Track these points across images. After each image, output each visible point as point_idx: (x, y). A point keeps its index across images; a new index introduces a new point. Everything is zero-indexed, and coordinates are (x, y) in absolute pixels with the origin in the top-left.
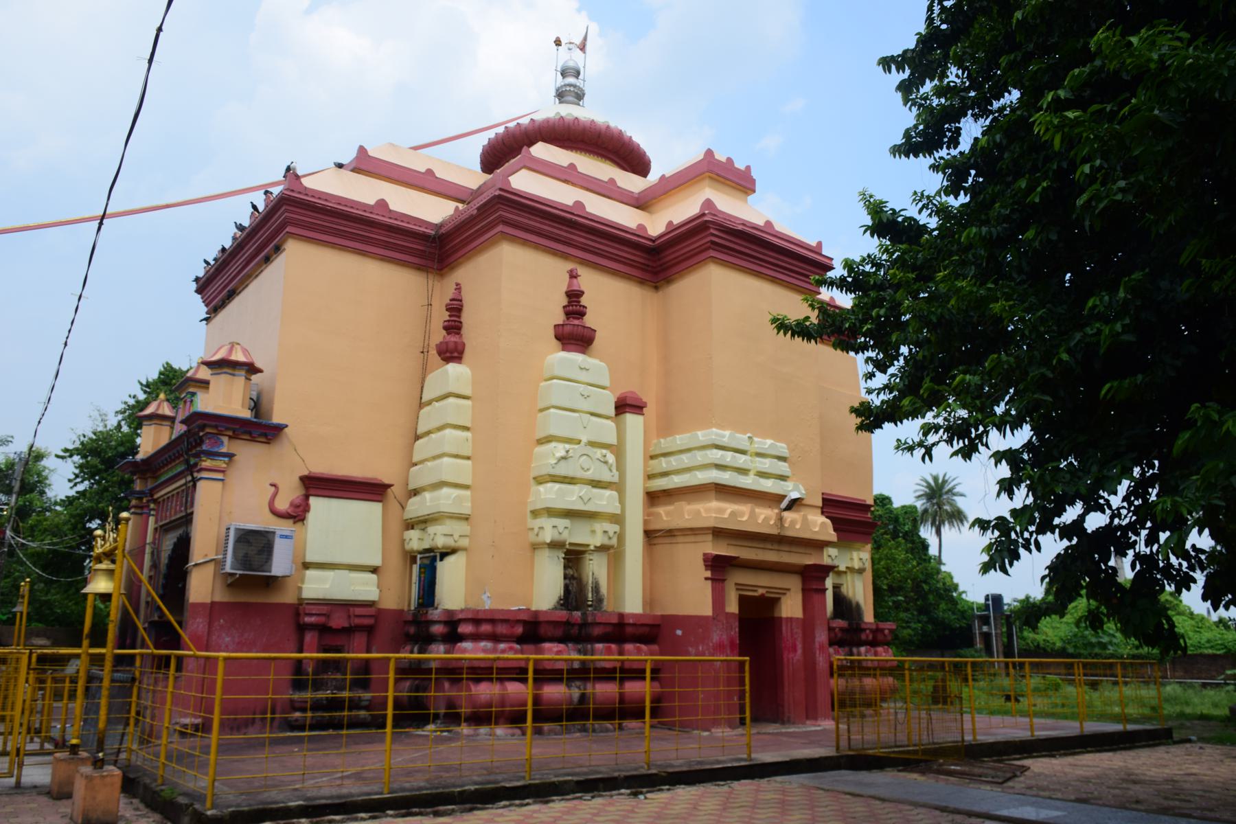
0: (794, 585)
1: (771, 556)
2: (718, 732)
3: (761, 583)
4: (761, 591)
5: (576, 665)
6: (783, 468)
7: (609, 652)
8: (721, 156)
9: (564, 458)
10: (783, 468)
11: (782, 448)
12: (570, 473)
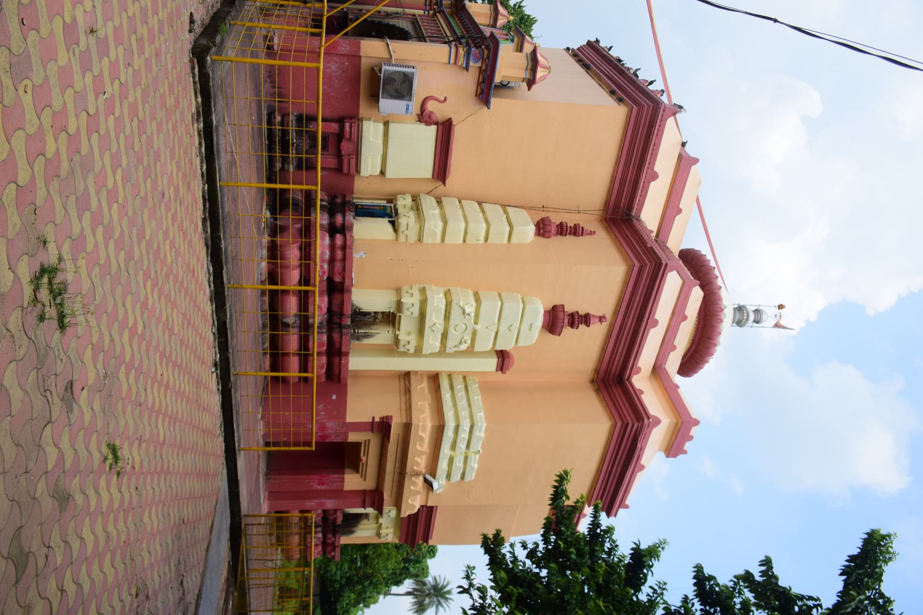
0: (369, 484)
1: (390, 466)
2: (261, 426)
3: (370, 459)
4: (364, 459)
5: (311, 321)
6: (456, 477)
7: (320, 345)
8: (694, 431)
9: (464, 312)
10: (456, 477)
11: (471, 476)
12: (452, 317)
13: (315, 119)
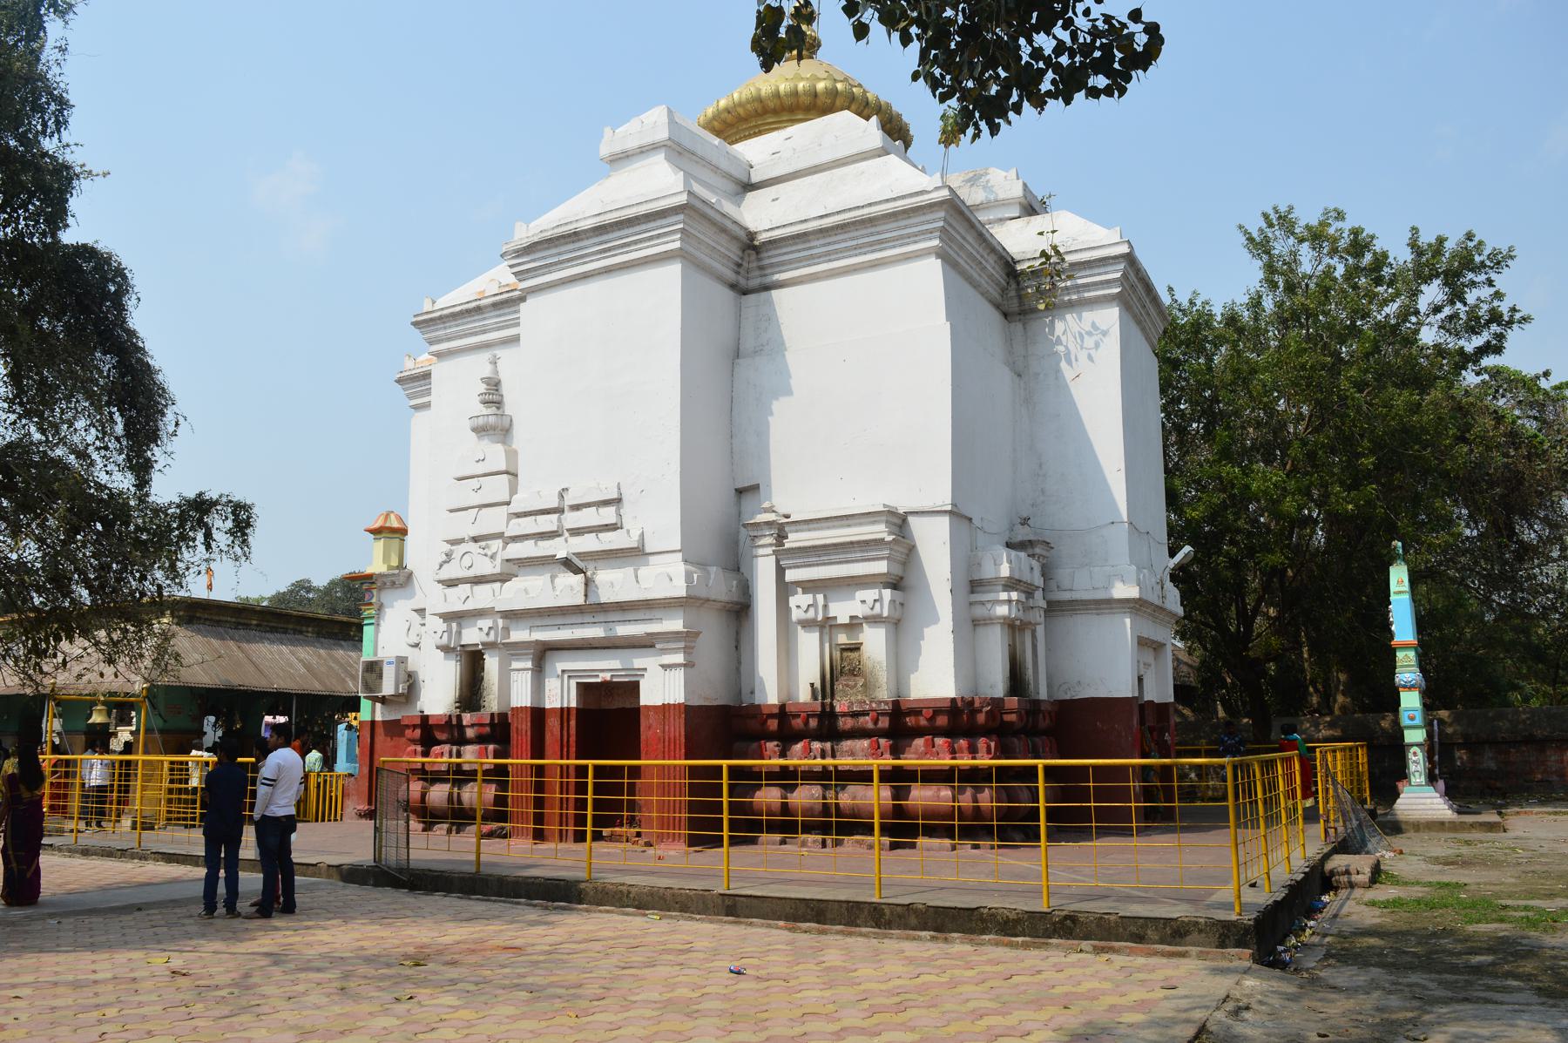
1: (595, 632)
3: (604, 667)
12: (454, 575)
13: (540, 770)
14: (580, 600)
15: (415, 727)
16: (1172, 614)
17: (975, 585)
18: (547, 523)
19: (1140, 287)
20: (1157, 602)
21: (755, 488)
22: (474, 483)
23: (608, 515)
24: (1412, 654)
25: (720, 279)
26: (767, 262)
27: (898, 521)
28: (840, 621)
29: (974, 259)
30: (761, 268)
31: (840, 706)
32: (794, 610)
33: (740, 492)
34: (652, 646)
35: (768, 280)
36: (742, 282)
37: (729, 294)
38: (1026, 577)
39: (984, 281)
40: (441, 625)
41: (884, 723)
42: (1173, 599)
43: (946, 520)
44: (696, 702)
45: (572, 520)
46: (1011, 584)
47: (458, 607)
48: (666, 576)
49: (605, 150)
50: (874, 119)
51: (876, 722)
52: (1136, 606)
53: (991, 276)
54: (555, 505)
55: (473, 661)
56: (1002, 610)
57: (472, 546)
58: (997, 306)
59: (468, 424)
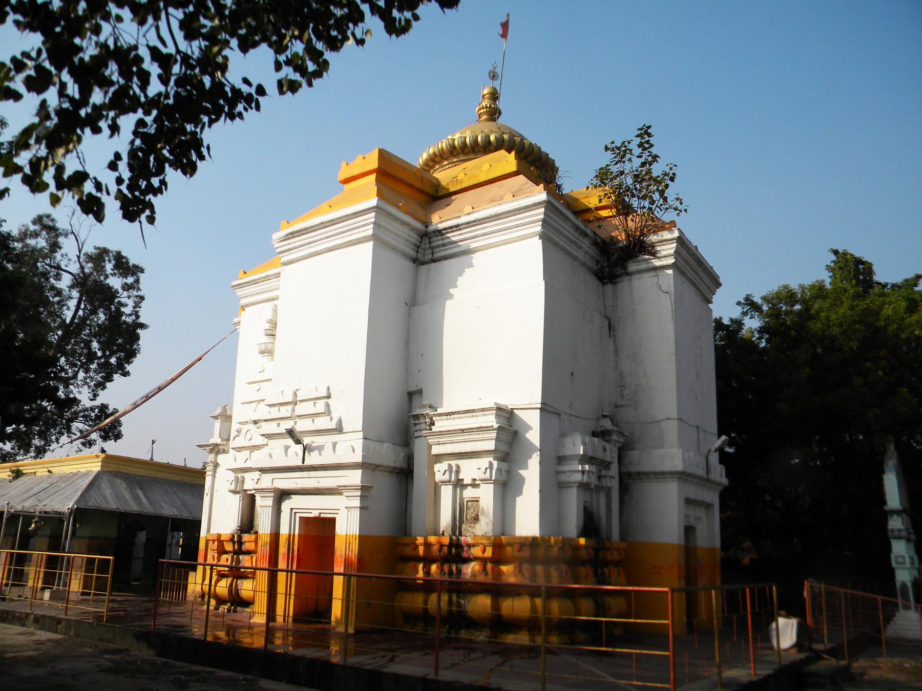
14: (300, 463)
15: (214, 541)
16: (719, 484)
17: (561, 459)
18: (285, 411)
19: (692, 262)
20: (702, 473)
21: (420, 392)
22: (256, 386)
23: (320, 406)
24: (336, 570)
25: (404, 254)
26: (435, 244)
27: (508, 415)
28: (465, 482)
29: (572, 242)
30: (432, 248)
31: (467, 539)
32: (437, 473)
33: (410, 395)
34: (341, 494)
35: (437, 255)
36: (420, 256)
37: (410, 265)
38: (600, 455)
39: (581, 255)
40: (232, 476)
41: (489, 553)
42: (719, 474)
43: (676, 421)
44: (365, 533)
45: (301, 409)
46: (584, 459)
47: (242, 465)
48: (351, 448)
49: (342, 176)
50: (513, 153)
51: (484, 551)
52: (683, 476)
53: (586, 253)
54: (291, 400)
55: (250, 502)
56: (578, 477)
57: (252, 427)
58: (595, 274)
59: (256, 350)
